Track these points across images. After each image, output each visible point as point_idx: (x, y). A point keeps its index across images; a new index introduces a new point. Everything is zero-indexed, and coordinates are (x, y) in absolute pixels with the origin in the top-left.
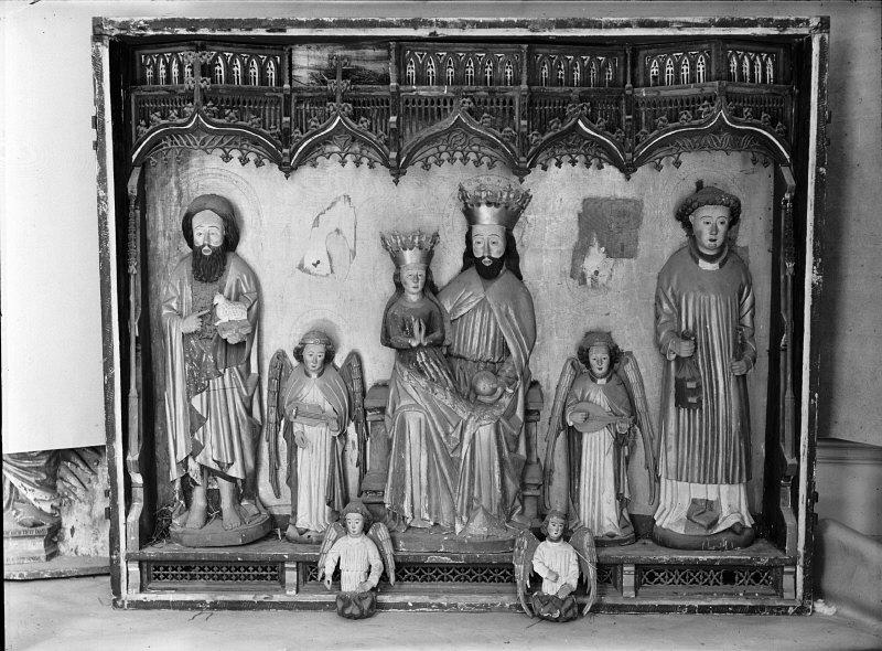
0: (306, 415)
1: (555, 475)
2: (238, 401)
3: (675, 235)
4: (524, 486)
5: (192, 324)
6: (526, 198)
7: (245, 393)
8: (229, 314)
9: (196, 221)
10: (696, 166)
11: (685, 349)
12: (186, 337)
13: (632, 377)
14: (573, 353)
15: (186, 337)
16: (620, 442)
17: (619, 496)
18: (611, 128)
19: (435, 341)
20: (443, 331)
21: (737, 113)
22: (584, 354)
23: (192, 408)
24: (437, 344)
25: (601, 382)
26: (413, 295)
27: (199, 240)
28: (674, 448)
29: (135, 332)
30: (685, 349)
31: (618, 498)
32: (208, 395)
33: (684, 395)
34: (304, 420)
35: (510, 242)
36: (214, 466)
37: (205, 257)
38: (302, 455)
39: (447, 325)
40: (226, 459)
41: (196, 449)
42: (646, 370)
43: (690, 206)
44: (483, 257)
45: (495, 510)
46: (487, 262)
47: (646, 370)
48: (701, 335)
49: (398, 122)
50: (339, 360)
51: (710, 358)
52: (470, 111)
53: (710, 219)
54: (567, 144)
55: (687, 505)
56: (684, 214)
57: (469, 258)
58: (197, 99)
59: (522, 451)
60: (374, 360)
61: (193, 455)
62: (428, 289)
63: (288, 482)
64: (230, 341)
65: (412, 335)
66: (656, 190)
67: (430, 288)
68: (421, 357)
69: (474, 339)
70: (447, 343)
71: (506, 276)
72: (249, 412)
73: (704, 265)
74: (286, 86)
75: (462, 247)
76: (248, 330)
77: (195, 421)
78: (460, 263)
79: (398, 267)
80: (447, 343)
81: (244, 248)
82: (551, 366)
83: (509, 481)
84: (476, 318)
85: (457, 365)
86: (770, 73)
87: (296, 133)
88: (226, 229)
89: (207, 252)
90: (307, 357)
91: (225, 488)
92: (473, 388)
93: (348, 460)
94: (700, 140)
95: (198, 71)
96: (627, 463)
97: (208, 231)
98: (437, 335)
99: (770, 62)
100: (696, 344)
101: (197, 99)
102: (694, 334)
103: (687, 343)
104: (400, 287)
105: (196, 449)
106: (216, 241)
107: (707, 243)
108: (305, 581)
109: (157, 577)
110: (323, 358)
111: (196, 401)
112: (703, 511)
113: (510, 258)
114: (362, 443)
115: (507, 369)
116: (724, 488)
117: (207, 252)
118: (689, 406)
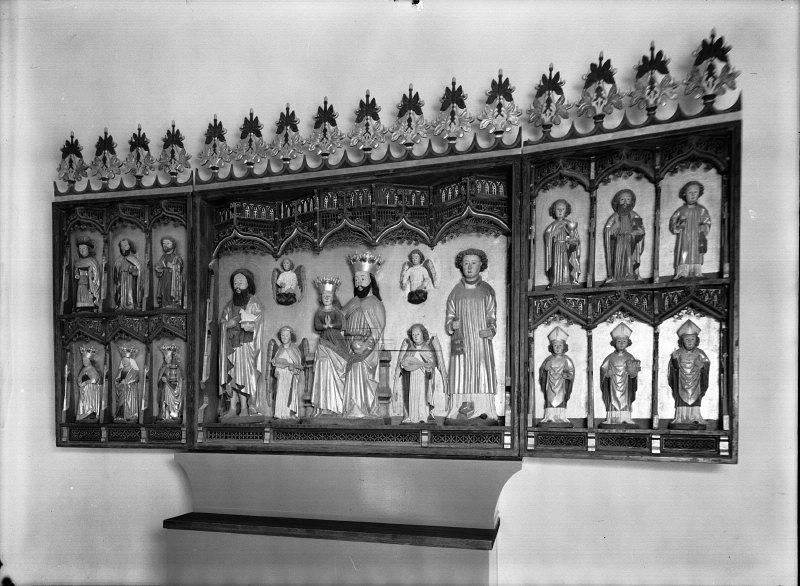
12: (228, 330)
16: (429, 376)
53: (472, 260)
67: (335, 302)
72: (256, 366)
83: (369, 392)
105: (229, 378)
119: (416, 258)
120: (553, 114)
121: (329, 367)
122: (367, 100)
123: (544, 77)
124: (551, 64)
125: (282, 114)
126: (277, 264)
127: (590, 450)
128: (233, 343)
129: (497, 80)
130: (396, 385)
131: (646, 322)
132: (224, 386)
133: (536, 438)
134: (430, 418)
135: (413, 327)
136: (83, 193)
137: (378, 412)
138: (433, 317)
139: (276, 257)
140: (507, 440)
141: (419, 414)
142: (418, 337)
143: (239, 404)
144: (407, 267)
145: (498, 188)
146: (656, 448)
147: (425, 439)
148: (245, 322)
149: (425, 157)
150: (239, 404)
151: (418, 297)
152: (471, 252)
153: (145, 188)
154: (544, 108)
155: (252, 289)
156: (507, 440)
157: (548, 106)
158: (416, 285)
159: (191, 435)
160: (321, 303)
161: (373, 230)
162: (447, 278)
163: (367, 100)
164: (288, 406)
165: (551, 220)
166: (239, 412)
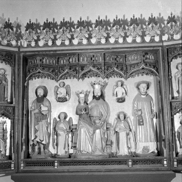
0: (60, 129)
2: (45, 127)
3: (136, 92)
4: (107, 145)
5: (37, 111)
8: (44, 108)
9: (38, 90)
10: (138, 79)
11: (139, 113)
12: (35, 114)
13: (129, 121)
14: (116, 117)
15: (35, 114)
16: (128, 134)
17: (128, 147)
18: (122, 70)
19: (87, 113)
21: (146, 65)
22: (119, 117)
23: (35, 128)
24: (87, 114)
26: (82, 104)
27: (38, 94)
29: (25, 113)
30: (139, 113)
31: (127, 147)
32: (39, 125)
33: (141, 122)
34: (59, 130)
35: (102, 92)
36: (40, 141)
37: (39, 97)
38: (60, 138)
39: (89, 110)
40: (42, 139)
41: (36, 137)
42: (132, 119)
43: (138, 84)
44: (96, 96)
46: (97, 97)
47: (132, 119)
48: (143, 110)
50: (67, 119)
53: (143, 87)
54: (113, 74)
55: (142, 148)
57: (94, 97)
58: (39, 66)
59: (106, 136)
61: (35, 139)
62: (85, 103)
63: (56, 145)
64: (44, 114)
65: (82, 111)
66: (131, 83)
67: (86, 102)
68: (84, 116)
69: (95, 113)
70: (89, 114)
71: (101, 99)
72: (47, 130)
73: (143, 96)
74: (57, 64)
75: (93, 95)
76: (48, 112)
77: (36, 131)
79: (79, 98)
80: (89, 114)
82: (112, 120)
83: (103, 142)
84: (96, 110)
85: (91, 118)
87: (59, 73)
90: (61, 117)
91: (42, 146)
92: (95, 123)
93: (69, 141)
94: (138, 73)
95: (39, 60)
97: (41, 92)
98: (87, 111)
101: (39, 66)
103: (140, 112)
104: (79, 102)
105: (36, 137)
106: (42, 94)
107: (143, 91)
109: (27, 166)
110: (64, 117)
111: (36, 127)
112: (146, 149)
113: (102, 96)
114: (72, 137)
116: (150, 143)
118: (141, 125)
120: (174, 30)
146: (130, 161)
147: (130, 163)
157: (172, 28)
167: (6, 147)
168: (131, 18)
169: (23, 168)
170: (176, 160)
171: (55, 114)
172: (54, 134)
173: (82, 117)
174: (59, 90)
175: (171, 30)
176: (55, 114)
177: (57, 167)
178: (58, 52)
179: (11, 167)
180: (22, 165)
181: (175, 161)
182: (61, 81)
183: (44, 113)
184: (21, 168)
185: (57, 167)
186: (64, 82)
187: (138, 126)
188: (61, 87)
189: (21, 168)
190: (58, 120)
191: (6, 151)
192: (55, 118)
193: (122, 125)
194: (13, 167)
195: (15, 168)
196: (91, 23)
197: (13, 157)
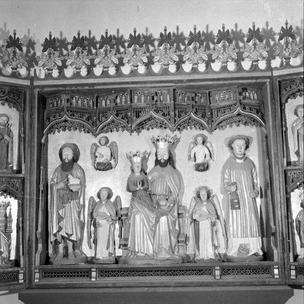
1: (190, 239)
2: (75, 213)
3: (227, 154)
4: (178, 242)
5: (61, 185)
6: (178, 140)
7: (78, 209)
8: (73, 181)
9: (63, 151)
11: (233, 189)
12: (58, 190)
13: (216, 202)
14: (194, 195)
15: (58, 190)
16: (213, 225)
17: (213, 245)
18: (203, 116)
20: (148, 185)
21: (244, 108)
22: (198, 196)
23: (59, 214)
24: (146, 190)
25: (205, 203)
27: (64, 157)
28: (232, 226)
29: (41, 188)
30: (233, 189)
32: (65, 209)
33: (235, 204)
34: (99, 217)
36: (66, 236)
37: (66, 163)
38: (100, 230)
39: (150, 184)
40: (70, 233)
41: (60, 229)
42: (220, 198)
45: (167, 249)
46: (162, 161)
47: (220, 198)
49: (131, 114)
50: (112, 200)
51: (242, 191)
52: (155, 110)
53: (239, 144)
54: (189, 123)
56: (230, 146)
57: (157, 162)
59: (177, 228)
60: (125, 199)
61: (58, 231)
63: (94, 242)
66: (219, 138)
67: (143, 171)
68: (140, 193)
69: (159, 189)
70: (149, 190)
72: (79, 218)
73: (238, 161)
74: (95, 107)
76: (80, 187)
77: (60, 219)
78: (154, 164)
79: (132, 164)
80: (149, 190)
81: (80, 162)
82: (187, 200)
83: (172, 237)
84: (161, 183)
86: (256, 97)
87: (98, 123)
88: (74, 154)
89: (67, 161)
90: (102, 196)
91: (70, 244)
92: (158, 205)
95: (66, 101)
96: (216, 233)
97: (68, 155)
98: (146, 186)
99: (255, 94)
100: (237, 187)
102: (236, 183)
105: (60, 229)
106: (70, 157)
108: (99, 276)
110: (107, 196)
111: (60, 212)
112: (243, 248)
113: (171, 161)
115: (171, 198)
117: (67, 161)
119: (200, 140)
120: (290, 51)
121: (140, 221)
122: (165, 33)
123: (282, 28)
124: (135, 28)
125: (46, 39)
126: (95, 140)
127: (292, 278)
128: (63, 202)
129: (105, 36)
130: (190, 231)
131: (84, 190)
132: (55, 235)
133: (296, 269)
134: (215, 255)
135: (201, 188)
136: (72, 78)
137: (180, 252)
138: (213, 180)
139: (96, 136)
140: (276, 271)
141: (207, 252)
142: (205, 196)
143: (66, 248)
144: (192, 146)
145: (253, 95)
146: (217, 270)
147: (218, 273)
148: (73, 185)
149: (72, 78)
150: (66, 248)
151: (203, 168)
152: (240, 137)
153: (293, 67)
154: (284, 48)
155: (75, 159)
156: (276, 271)
157: (287, 47)
158: (200, 160)
159: (29, 277)
160: (133, 171)
161: (94, 124)
162: (222, 155)
163: (165, 33)
164: (107, 249)
165: (295, 117)
166: (66, 255)
167: (9, 245)
168: (282, 27)
169: (38, 281)
170: (293, 267)
171: (91, 191)
172: (89, 225)
173: (137, 195)
174: (99, 150)
175: (285, 49)
176: (91, 191)
177: (94, 280)
178: (96, 87)
179: (18, 280)
180: (37, 275)
181: (293, 269)
182: (102, 135)
183: (74, 189)
184: (36, 281)
185: (94, 280)
186: (106, 138)
187: (230, 211)
188: (102, 145)
189: (36, 281)
190: (97, 200)
191: (9, 252)
192: (92, 197)
193: (204, 209)
194: (21, 280)
195: (25, 281)
196: (152, 39)
197: (22, 262)
